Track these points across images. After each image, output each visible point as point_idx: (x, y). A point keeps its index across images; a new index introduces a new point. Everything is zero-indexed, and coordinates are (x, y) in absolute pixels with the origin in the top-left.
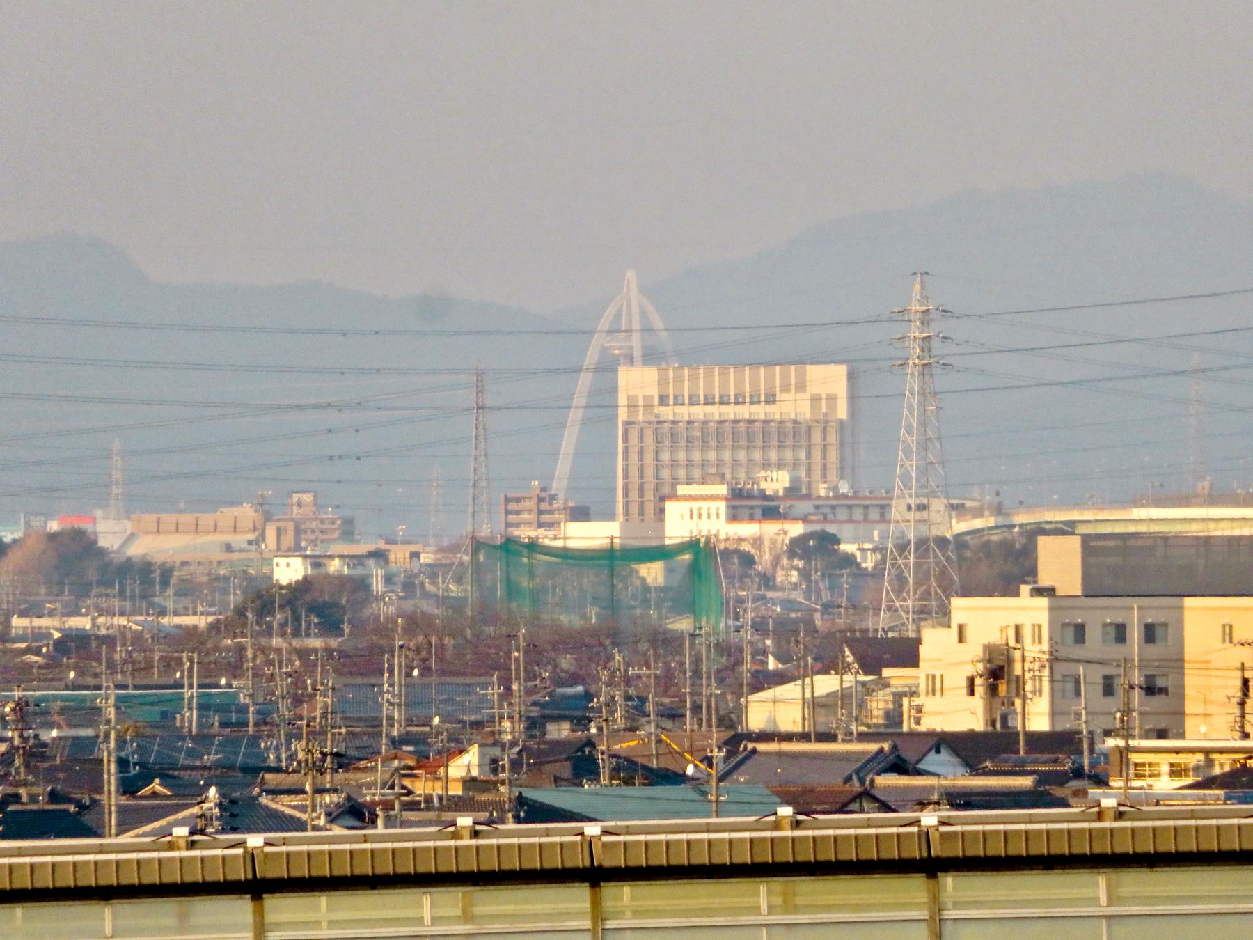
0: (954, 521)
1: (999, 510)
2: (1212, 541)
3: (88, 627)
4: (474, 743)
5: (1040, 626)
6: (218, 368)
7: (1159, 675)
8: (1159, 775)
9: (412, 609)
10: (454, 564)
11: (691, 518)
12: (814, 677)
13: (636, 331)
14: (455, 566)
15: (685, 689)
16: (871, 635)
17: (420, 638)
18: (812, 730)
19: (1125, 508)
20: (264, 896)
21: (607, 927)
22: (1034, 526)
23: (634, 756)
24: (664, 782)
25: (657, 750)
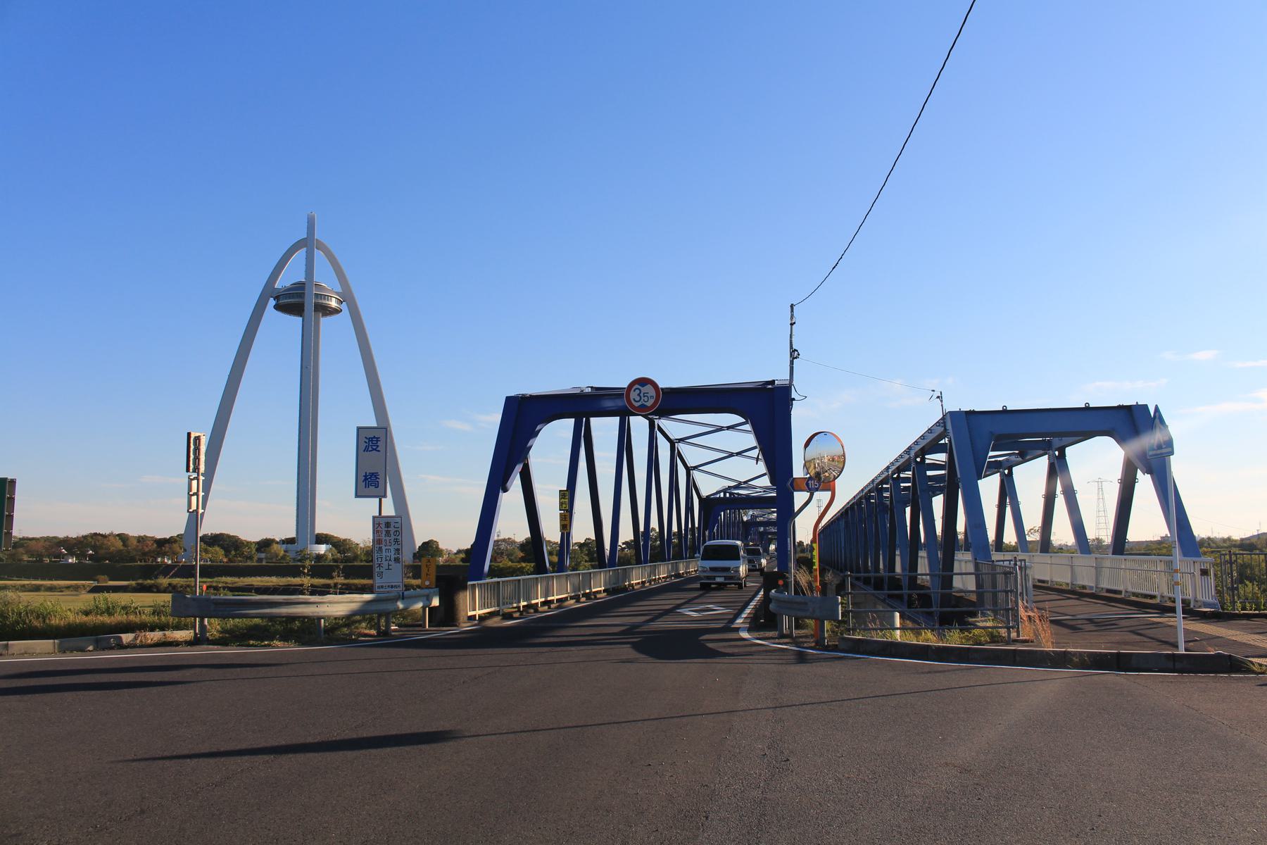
0: (282, 553)
1: (1217, 677)
2: (1261, 537)
3: (814, 567)
4: (377, 541)
5: (198, 439)
6: (1155, 626)
7: (303, 321)
8: (1026, 611)
9: (130, 544)
10: (591, 565)
11: (1229, 665)
12: (974, 576)
13: (1174, 665)
14: (593, 563)
15: (655, 576)
16: (597, 563)
17: (289, 626)
18: (953, 590)
19: (352, 611)
20: (1198, 539)
21: (1107, 536)
22: (839, 514)
23: (704, 594)
24: (1254, 541)
25: (195, 620)
